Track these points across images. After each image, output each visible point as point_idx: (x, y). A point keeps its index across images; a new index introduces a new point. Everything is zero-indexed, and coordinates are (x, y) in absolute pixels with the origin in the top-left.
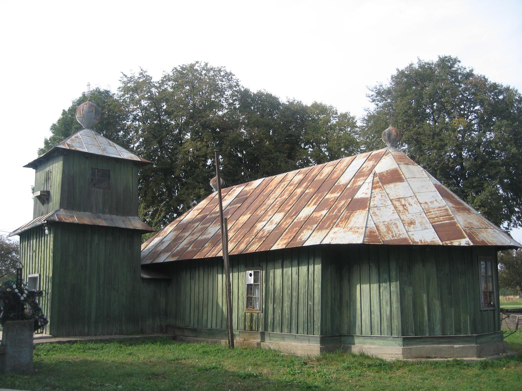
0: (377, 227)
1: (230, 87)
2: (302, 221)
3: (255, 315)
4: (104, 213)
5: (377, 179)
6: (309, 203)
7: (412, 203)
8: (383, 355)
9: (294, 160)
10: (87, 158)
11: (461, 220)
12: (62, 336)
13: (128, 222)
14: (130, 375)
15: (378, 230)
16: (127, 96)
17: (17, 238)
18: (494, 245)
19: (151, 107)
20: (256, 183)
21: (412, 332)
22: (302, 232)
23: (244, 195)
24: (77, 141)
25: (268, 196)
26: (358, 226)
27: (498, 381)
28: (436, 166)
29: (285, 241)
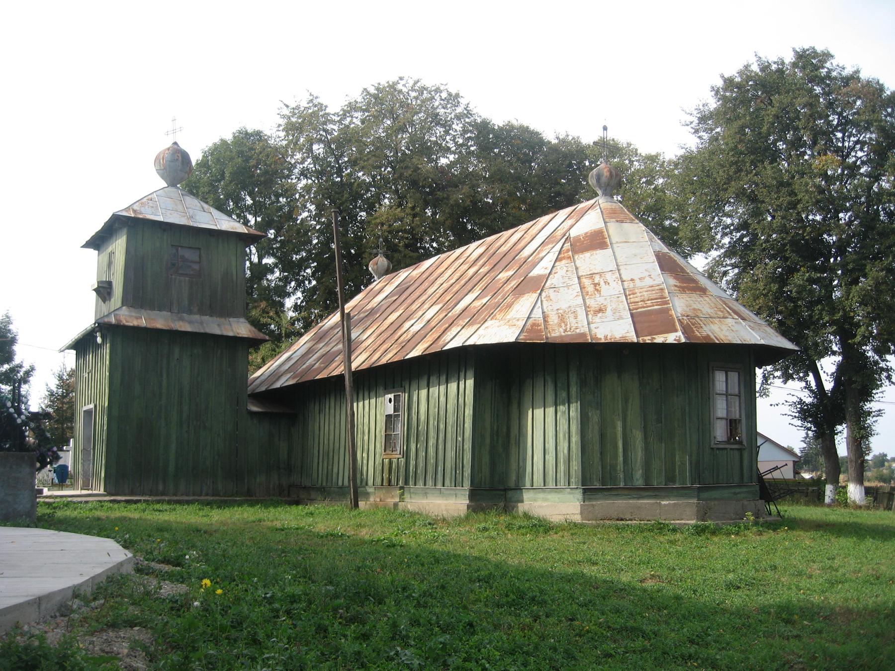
3: (395, 461)
4: (190, 312)
5: (567, 245)
10: (164, 230)
21: (598, 478)
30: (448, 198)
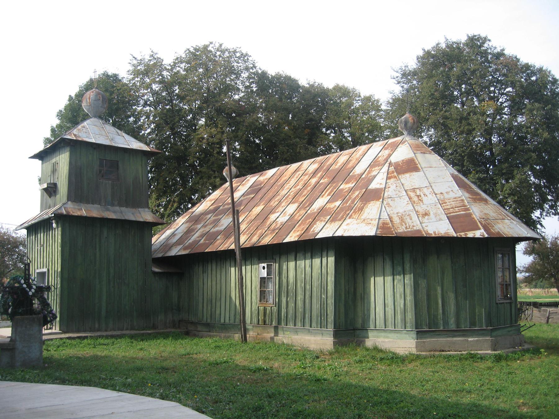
0: (390, 218)
1: (247, 69)
2: (315, 213)
3: (268, 309)
4: (113, 205)
5: (392, 169)
6: (324, 193)
7: (427, 193)
8: (397, 349)
9: (315, 146)
10: (95, 149)
11: (477, 211)
12: (72, 332)
13: (138, 215)
14: (140, 369)
15: (391, 221)
16: (136, 79)
17: (25, 232)
18: (510, 236)
19: (163, 91)
20: (270, 173)
21: (426, 324)
22: (315, 224)
23: (258, 185)
24: (84, 130)
25: (282, 186)
26: (371, 217)
27: (509, 373)
28: (463, 152)
29: (298, 233)
30: (244, 121)
